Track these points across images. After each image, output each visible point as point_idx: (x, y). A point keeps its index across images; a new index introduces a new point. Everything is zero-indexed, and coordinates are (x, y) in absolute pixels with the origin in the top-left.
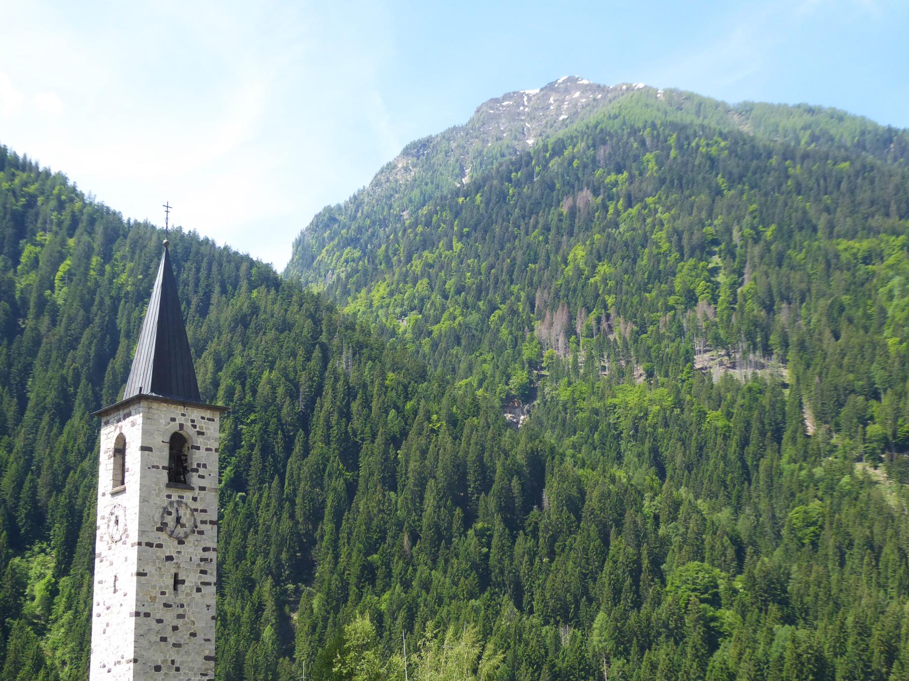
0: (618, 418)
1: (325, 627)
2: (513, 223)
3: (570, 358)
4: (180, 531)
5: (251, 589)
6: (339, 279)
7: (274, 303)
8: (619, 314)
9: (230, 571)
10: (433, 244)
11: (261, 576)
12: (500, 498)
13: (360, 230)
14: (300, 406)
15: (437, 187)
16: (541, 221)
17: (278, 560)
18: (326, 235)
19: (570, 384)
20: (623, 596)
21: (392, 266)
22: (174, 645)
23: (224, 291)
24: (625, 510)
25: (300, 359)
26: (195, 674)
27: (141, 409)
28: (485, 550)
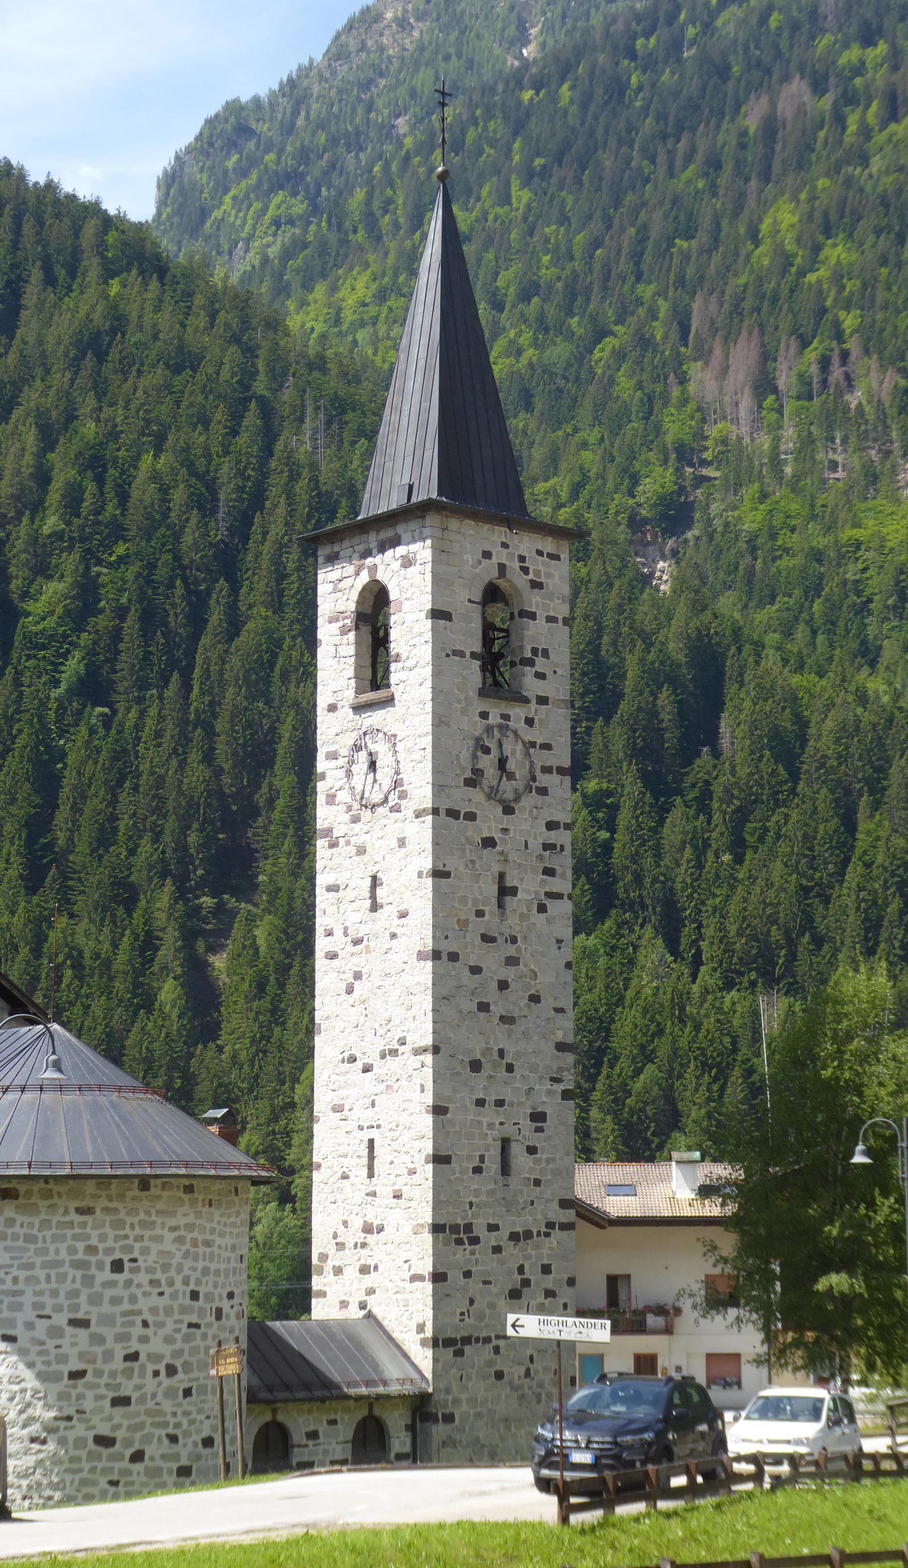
0: (865, 570)
1: (282, 985)
2: (643, 150)
3: (765, 441)
4: (508, 788)
5: (130, 903)
6: (265, 261)
7: (157, 309)
8: (867, 352)
9: (84, 867)
10: (468, 192)
11: (150, 879)
12: (635, 731)
13: (304, 155)
14: (219, 530)
15: (470, 65)
16: (703, 146)
17: (181, 846)
18: (230, 164)
19: (764, 496)
20: (884, 934)
21: (379, 238)
22: (502, 1018)
23: (50, 280)
24: (889, 761)
25: (218, 429)
26: (541, 1078)
27: (427, 531)
28: (604, 835)
